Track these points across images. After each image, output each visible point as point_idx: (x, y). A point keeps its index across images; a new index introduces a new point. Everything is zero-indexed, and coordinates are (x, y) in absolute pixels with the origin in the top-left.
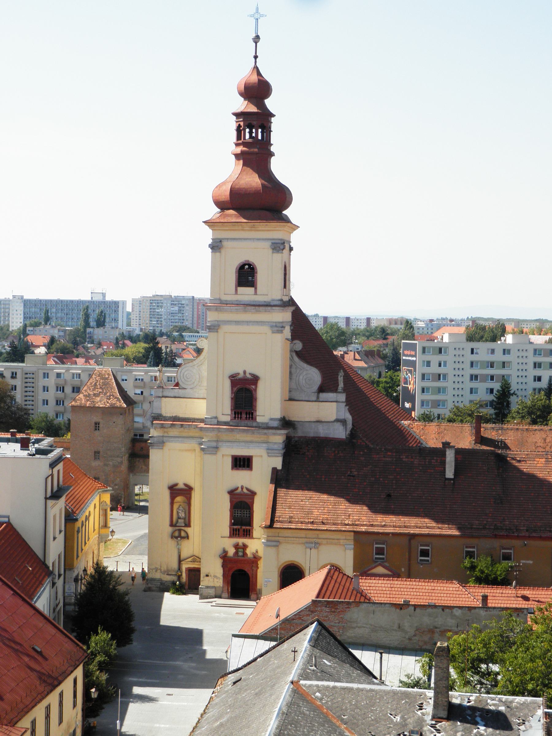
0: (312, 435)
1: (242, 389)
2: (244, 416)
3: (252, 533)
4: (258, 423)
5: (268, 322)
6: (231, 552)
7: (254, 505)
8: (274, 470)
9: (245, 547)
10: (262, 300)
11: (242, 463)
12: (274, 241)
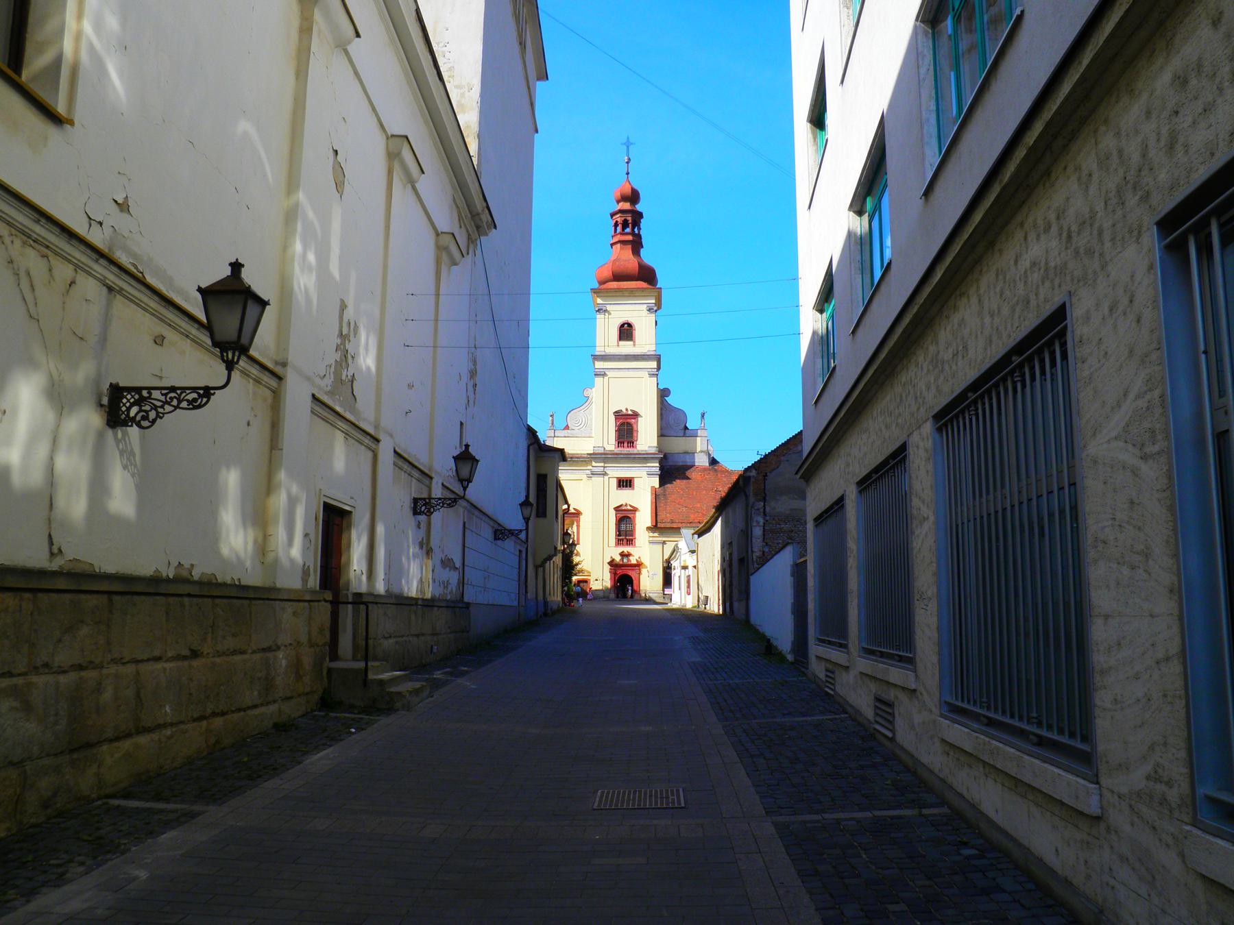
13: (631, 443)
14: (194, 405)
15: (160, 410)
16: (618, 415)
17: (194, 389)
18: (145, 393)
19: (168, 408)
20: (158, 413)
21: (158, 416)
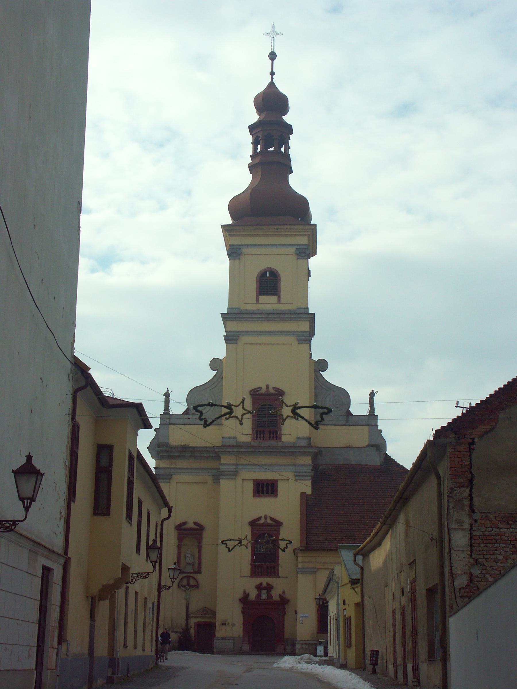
2: (267, 435)
5: (294, 332)
6: (253, 594)
8: (303, 494)
9: (269, 587)
10: (286, 308)
12: (298, 247)
14: (145, 577)
17: (145, 573)
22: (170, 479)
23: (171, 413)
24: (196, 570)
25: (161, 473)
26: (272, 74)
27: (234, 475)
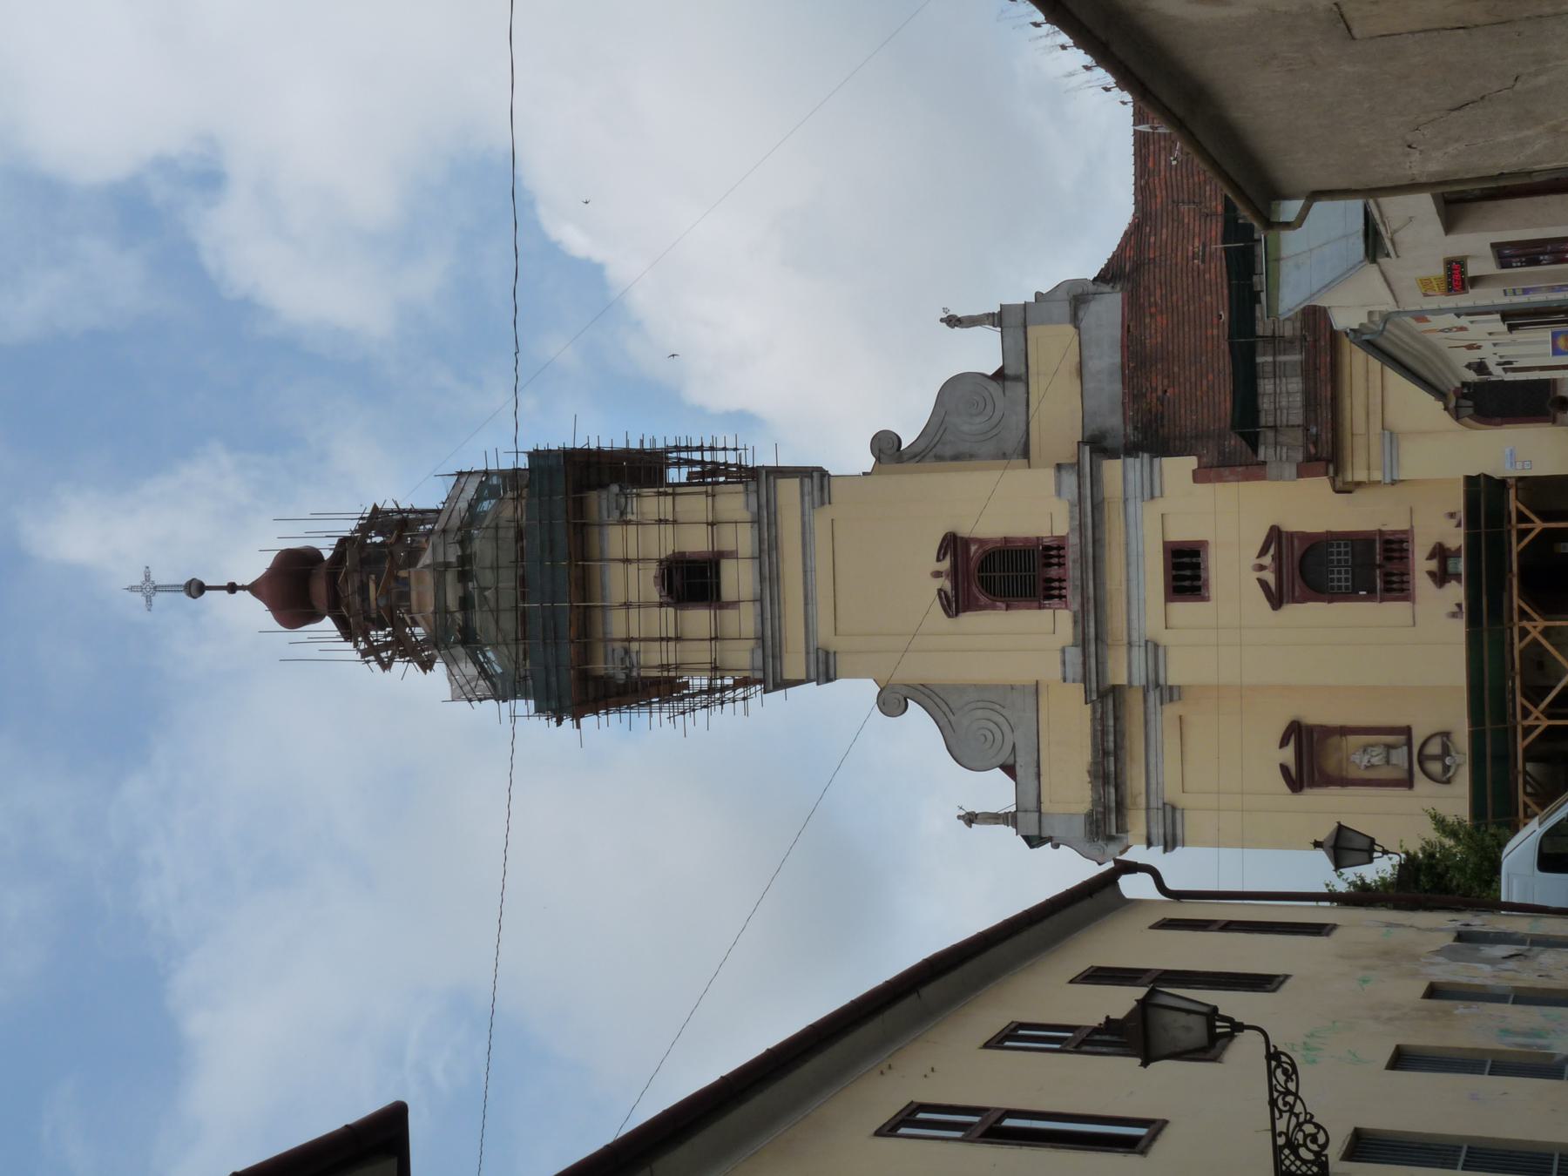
0: (1118, 387)
1: (981, 579)
2: (1054, 572)
3: (1394, 532)
4: (1072, 530)
7: (1308, 530)
8: (1198, 477)
9: (1440, 553)
11: (1188, 573)
13: (1051, 552)
14: (1292, 1072)
15: (1302, 1119)
16: (956, 603)
17: (1271, 1074)
18: (1281, 1141)
19: (1298, 1108)
20: (1306, 1121)
21: (1310, 1121)
22: (1174, 808)
23: (1013, 809)
24: (1402, 738)
25: (1161, 831)
26: (232, 588)
27: (1154, 649)
